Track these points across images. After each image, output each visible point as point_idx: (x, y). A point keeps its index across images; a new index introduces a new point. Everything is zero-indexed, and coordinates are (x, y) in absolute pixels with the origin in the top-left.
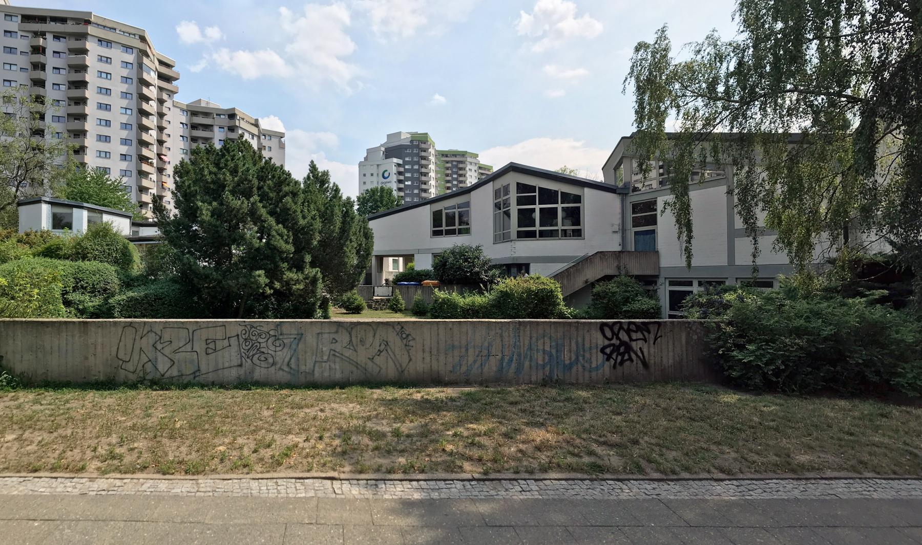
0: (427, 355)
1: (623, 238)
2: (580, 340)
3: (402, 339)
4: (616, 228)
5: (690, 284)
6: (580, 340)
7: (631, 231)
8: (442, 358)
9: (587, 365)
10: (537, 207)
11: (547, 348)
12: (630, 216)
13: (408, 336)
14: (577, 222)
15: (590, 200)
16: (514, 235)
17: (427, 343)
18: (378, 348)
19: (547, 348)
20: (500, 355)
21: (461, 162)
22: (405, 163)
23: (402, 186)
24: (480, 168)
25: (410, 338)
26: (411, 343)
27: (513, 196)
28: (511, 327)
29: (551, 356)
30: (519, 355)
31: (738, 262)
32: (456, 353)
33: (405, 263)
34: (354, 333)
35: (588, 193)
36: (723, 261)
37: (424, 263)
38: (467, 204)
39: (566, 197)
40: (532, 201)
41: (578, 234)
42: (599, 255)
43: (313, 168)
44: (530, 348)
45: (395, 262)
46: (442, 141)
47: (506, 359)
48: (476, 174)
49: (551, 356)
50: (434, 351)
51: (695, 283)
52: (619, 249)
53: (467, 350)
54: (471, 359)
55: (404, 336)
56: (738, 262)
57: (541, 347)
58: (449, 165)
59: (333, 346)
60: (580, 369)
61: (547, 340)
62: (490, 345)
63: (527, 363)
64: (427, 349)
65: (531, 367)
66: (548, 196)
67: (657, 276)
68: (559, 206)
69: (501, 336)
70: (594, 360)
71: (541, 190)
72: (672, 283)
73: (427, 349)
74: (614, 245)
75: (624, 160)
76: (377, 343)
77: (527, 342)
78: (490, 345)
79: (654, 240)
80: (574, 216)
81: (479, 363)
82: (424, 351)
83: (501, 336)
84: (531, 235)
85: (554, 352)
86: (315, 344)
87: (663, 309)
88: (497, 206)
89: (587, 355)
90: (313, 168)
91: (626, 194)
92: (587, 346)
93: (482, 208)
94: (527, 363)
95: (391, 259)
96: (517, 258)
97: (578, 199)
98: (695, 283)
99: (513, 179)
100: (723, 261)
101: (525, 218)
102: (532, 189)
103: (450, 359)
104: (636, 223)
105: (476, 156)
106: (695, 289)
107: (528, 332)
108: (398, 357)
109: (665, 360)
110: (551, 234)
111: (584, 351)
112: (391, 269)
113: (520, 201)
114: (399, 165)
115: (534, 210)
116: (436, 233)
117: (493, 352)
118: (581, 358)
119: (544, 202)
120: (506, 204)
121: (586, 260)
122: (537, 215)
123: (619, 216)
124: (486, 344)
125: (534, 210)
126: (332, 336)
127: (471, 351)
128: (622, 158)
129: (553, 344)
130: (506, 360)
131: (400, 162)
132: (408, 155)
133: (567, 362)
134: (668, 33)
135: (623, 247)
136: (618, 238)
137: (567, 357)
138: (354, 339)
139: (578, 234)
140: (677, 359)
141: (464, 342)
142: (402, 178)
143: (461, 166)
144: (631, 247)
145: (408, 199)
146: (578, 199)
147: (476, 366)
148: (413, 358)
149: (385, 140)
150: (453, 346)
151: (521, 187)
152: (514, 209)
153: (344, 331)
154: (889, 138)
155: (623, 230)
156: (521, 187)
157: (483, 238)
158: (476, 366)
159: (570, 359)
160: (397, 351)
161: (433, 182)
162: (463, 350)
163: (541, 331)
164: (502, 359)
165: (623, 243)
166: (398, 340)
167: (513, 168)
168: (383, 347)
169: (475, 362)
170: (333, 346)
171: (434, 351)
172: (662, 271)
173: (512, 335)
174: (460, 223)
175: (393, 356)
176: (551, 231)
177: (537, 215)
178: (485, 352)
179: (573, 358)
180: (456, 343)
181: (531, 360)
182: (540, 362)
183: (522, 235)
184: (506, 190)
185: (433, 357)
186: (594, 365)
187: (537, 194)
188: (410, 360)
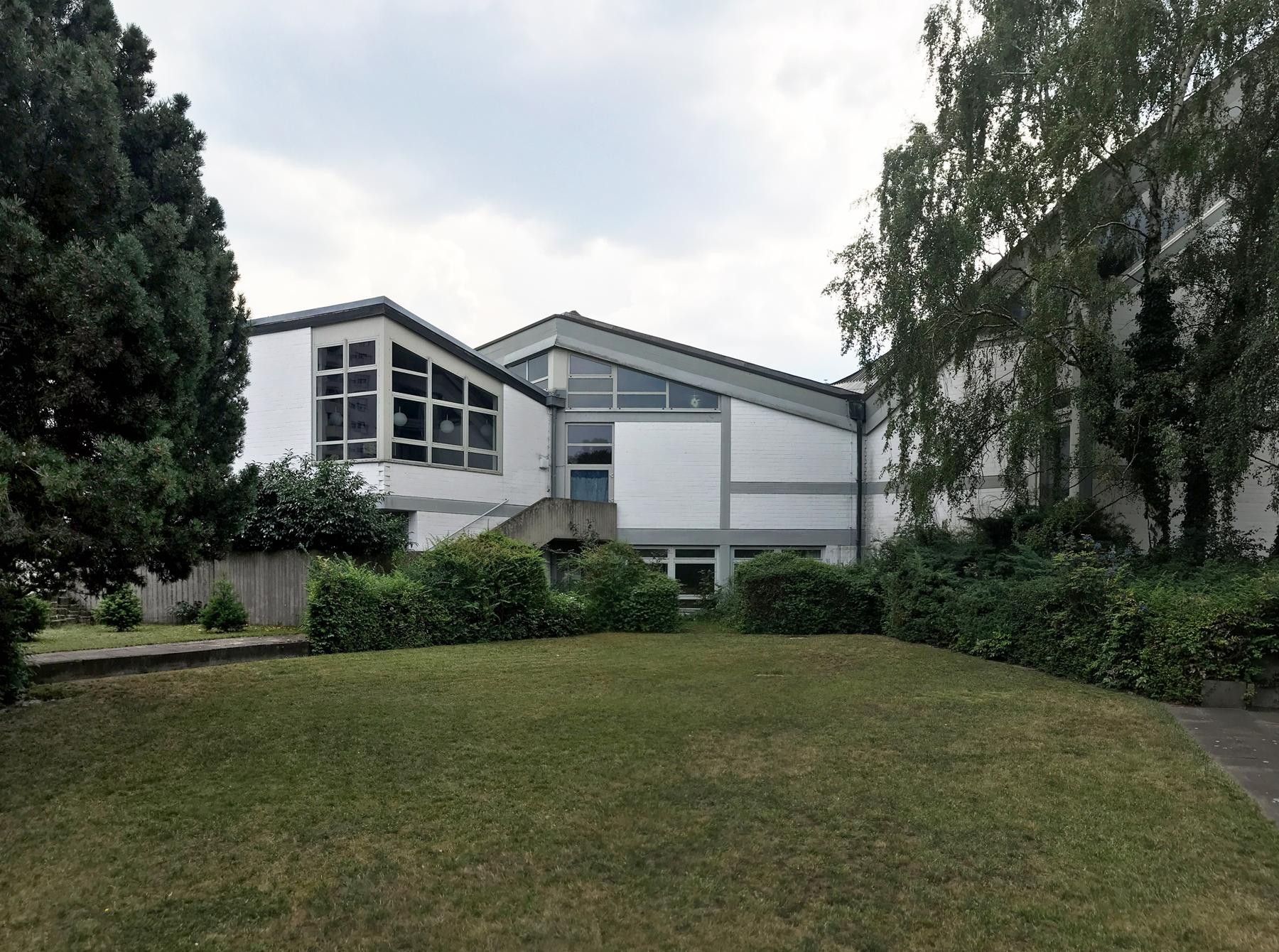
4: (546, 462)
5: (710, 554)
7: (566, 470)
14: (489, 442)
27: (383, 367)
31: (734, 524)
36: (713, 522)
39: (480, 397)
43: (182, 102)
56: (734, 524)
66: (448, 384)
71: (437, 370)
72: (740, 553)
79: (606, 488)
80: (485, 429)
84: (416, 455)
90: (182, 102)
97: (487, 400)
99: (380, 333)
102: (420, 364)
110: (442, 458)
113: (399, 383)
115: (462, 402)
125: (462, 402)
134: (841, 344)
136: (545, 479)
139: (486, 464)
151: (401, 356)
154: (989, 445)
155: (554, 468)
167: (383, 310)
183: (402, 453)
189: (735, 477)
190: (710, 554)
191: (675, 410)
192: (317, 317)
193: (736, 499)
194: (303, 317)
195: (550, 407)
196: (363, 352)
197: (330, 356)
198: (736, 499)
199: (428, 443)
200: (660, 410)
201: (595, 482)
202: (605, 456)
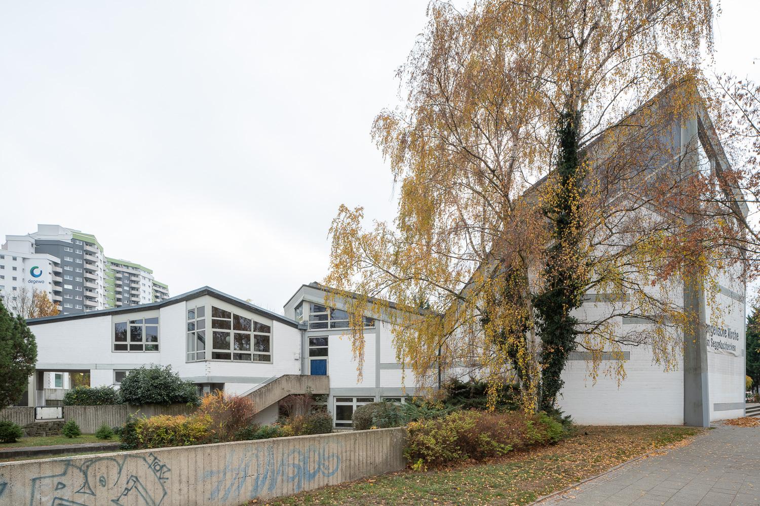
0: (184, 486)
1: (303, 365)
2: (321, 451)
3: (155, 471)
4: (297, 356)
6: (321, 451)
7: (309, 359)
8: (200, 487)
9: (326, 472)
10: (232, 332)
11: (296, 462)
12: (308, 347)
13: (162, 467)
15: (279, 332)
16: (209, 356)
17: (185, 472)
18: (125, 486)
19: (296, 462)
20: (256, 474)
21: (134, 275)
22: (64, 264)
23: (59, 289)
24: (155, 285)
25: (165, 469)
26: (167, 475)
27: (208, 318)
28: (266, 446)
29: (299, 468)
30: (273, 472)
31: (383, 385)
32: (214, 479)
33: (73, 383)
34: (90, 472)
35: (276, 326)
37: (102, 380)
38: (156, 321)
40: (226, 325)
41: (156, 348)
42: (285, 377)
44: (283, 464)
45: (58, 377)
46: (114, 246)
47: (261, 477)
48: (150, 290)
49: (299, 468)
50: (192, 481)
51: (355, 400)
52: (299, 373)
53: (225, 474)
54: (228, 483)
55: (158, 468)
57: (291, 462)
58: (120, 275)
59: (59, 494)
60: (321, 476)
61: (296, 454)
62: (247, 466)
63: (279, 479)
64: (184, 479)
65: (283, 481)
67: (328, 395)
68: (252, 334)
69: (257, 456)
70: (331, 466)
71: (237, 317)
72: (338, 400)
73: (184, 479)
74: (295, 370)
75: (304, 303)
76: (123, 479)
77: (280, 459)
78: (247, 466)
80: (264, 343)
81: (236, 485)
82: (180, 482)
83: (257, 456)
85: (301, 464)
86: (28, 494)
87: (332, 420)
88: (191, 327)
89: (326, 463)
91: (305, 330)
92: (326, 456)
93: (172, 326)
94: (279, 479)
95: (53, 374)
96: (212, 378)
97: (267, 329)
98: (355, 400)
99: (208, 303)
100: (373, 385)
101: (220, 341)
102: (228, 315)
103: (208, 487)
104: (312, 353)
105: (150, 272)
106: (354, 404)
107: (281, 450)
108: (151, 493)
109: (377, 459)
111: (324, 459)
112: (53, 385)
113: (215, 324)
114: (56, 264)
115: (228, 334)
116: (118, 348)
117: (250, 473)
118: (322, 466)
119: (235, 329)
120: (202, 324)
121: (275, 382)
122: (231, 339)
123: (299, 347)
124: (243, 466)
125: (228, 334)
126: (56, 480)
127: (228, 475)
128: (303, 301)
129: (302, 457)
130: (261, 479)
131: (58, 261)
132: (69, 255)
133: (312, 472)
135: (302, 373)
136: (298, 365)
137: (312, 467)
138: (90, 479)
139: (267, 359)
140: (384, 457)
141: (222, 467)
142: (59, 279)
143: (133, 278)
144: (308, 372)
145: (68, 306)
146: (267, 329)
147: (234, 489)
148: (168, 491)
149: (36, 230)
150: (212, 472)
151: (216, 311)
152: (209, 332)
153: (76, 471)
155: (303, 359)
156: (216, 311)
157: (174, 355)
158: (234, 489)
159: (314, 469)
160: (149, 487)
161: (101, 291)
162: (221, 475)
163: (291, 448)
164: (258, 478)
165: (302, 369)
166: (150, 472)
167: (207, 292)
168: (131, 483)
169: (232, 484)
170: (59, 494)
171: (192, 481)
172: (331, 390)
173: (266, 454)
174: (133, 339)
175: (144, 493)
176: (264, 355)
177: (231, 339)
178: (242, 474)
179: (317, 467)
180: (215, 469)
181: (283, 475)
182: (291, 475)
183: (217, 356)
184: (201, 310)
185: (191, 487)
186: (331, 471)
187: (232, 320)
188: (165, 494)
189: (394, 360)
190: (351, 400)
191: (333, 329)
192: (188, 296)
193: (382, 372)
194: (183, 296)
195: (300, 329)
196: (201, 310)
197: (191, 312)
198: (382, 372)
199: (144, 343)
200: (347, 328)
201: (199, 355)
202: (325, 352)
